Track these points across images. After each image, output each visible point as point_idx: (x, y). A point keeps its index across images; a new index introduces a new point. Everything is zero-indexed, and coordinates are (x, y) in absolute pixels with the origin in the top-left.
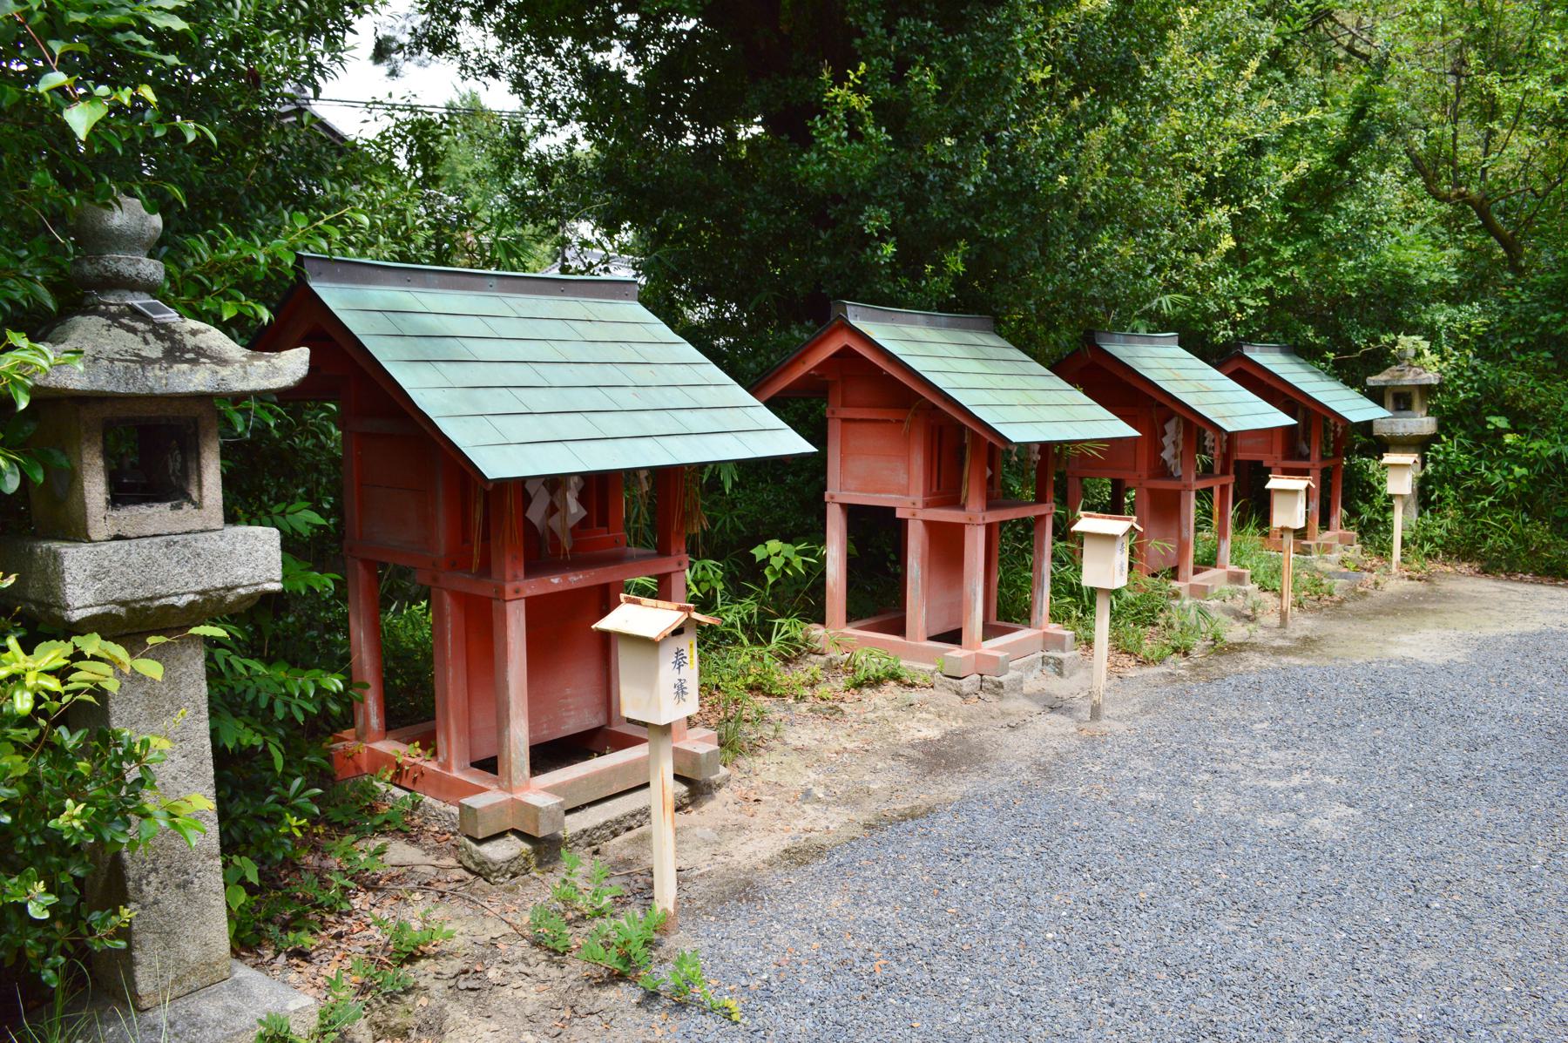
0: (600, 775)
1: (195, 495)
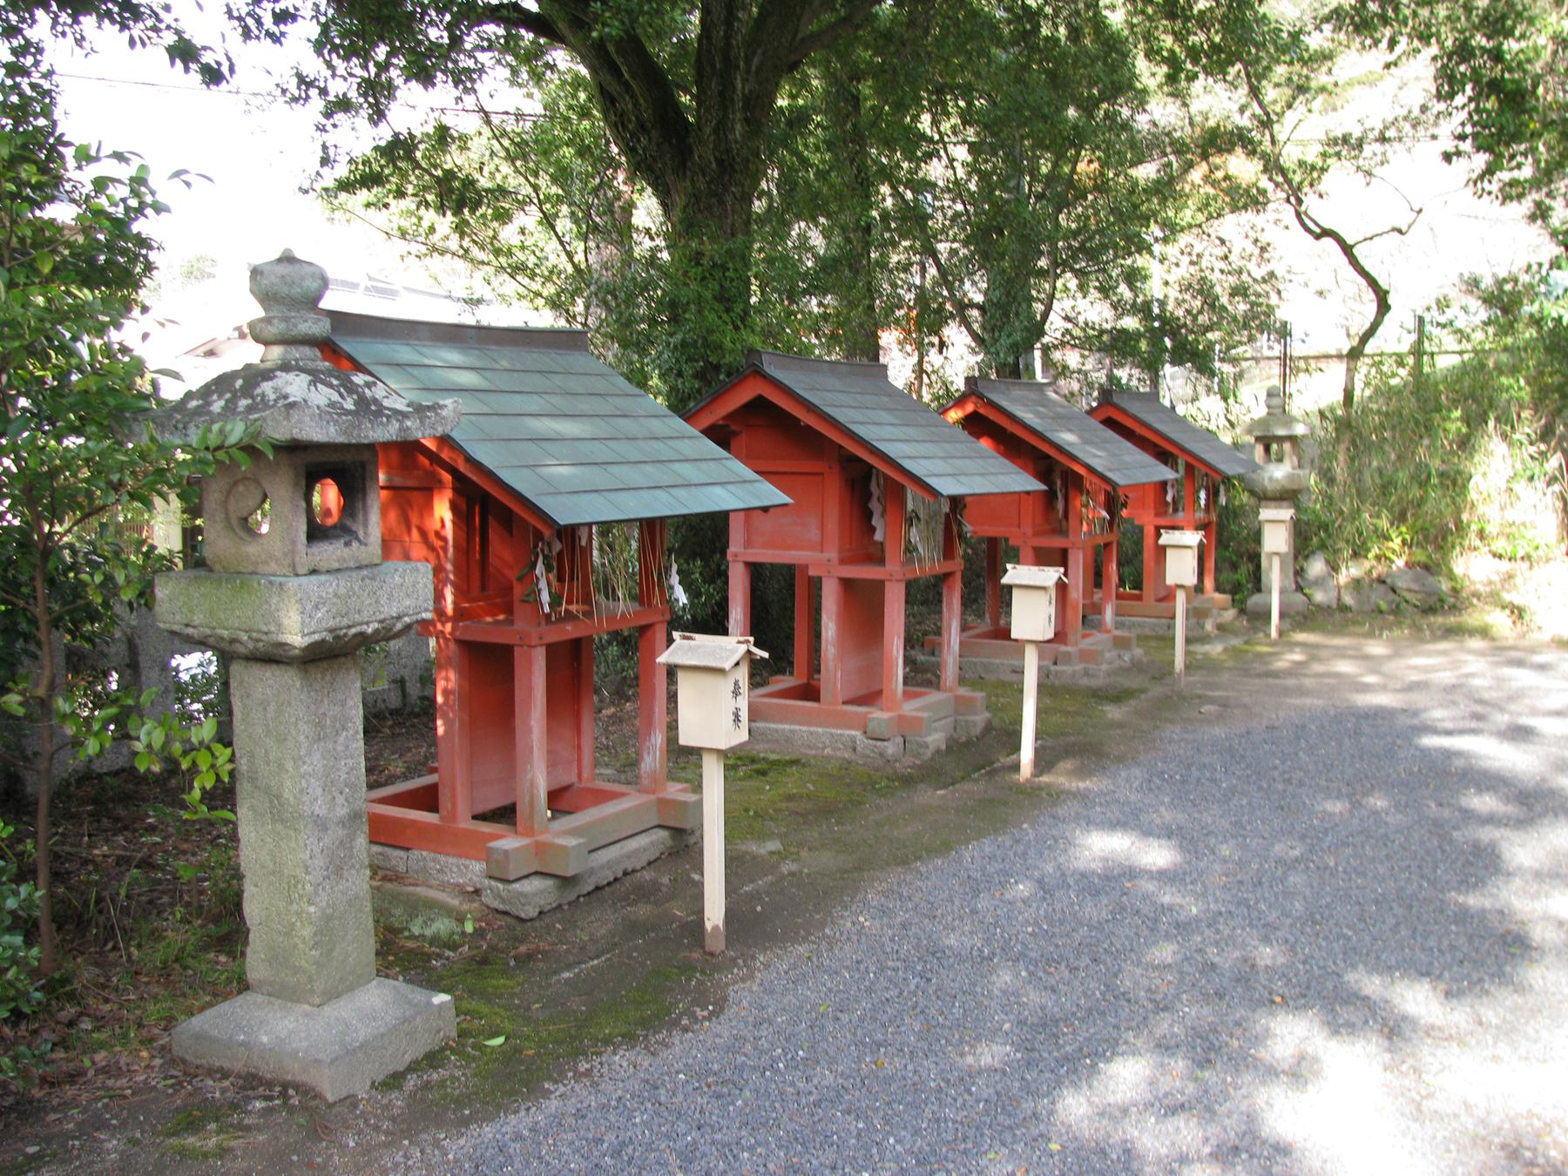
0: (617, 816)
1: (361, 534)
